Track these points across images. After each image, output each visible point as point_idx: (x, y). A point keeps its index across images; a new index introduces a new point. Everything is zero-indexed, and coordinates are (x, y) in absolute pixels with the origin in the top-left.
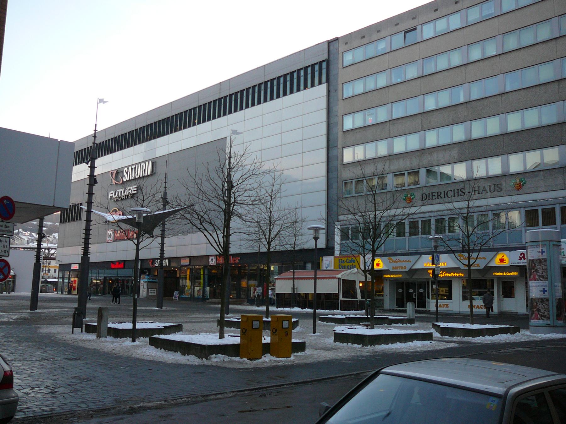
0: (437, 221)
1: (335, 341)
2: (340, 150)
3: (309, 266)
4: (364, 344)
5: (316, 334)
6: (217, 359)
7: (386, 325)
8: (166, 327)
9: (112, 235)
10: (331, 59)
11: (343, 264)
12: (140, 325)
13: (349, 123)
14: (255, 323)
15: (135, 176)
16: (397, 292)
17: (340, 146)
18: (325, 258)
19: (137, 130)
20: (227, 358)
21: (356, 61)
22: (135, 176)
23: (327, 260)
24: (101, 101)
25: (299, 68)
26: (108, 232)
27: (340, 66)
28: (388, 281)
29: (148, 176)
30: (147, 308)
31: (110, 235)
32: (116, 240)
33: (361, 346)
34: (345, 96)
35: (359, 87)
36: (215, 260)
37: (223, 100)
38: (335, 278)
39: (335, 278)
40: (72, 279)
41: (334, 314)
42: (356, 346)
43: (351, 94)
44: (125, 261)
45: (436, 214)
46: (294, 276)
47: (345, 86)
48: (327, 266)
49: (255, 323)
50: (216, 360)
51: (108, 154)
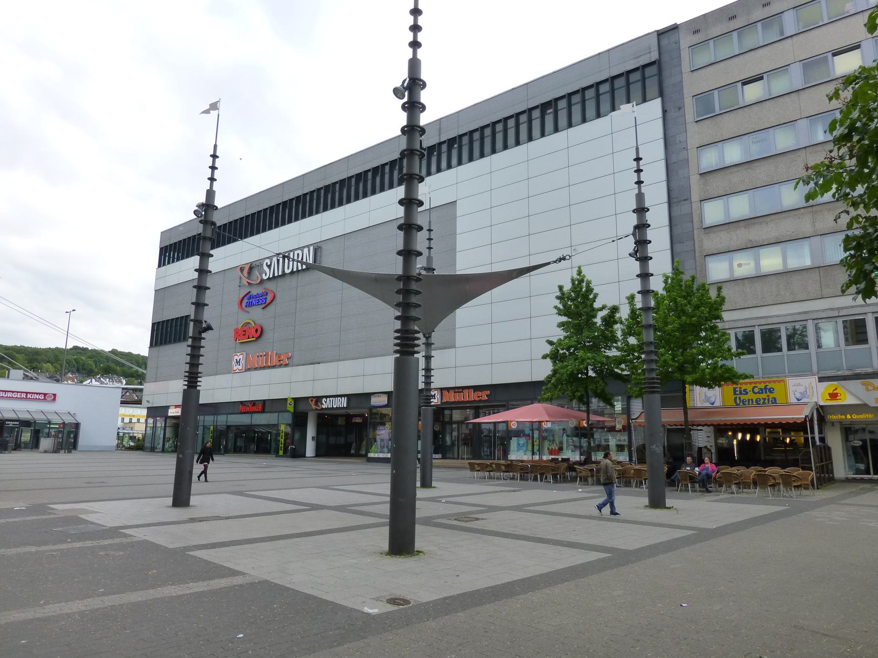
0: (764, 334)
2: (695, 206)
10: (665, 58)
11: (743, 397)
15: (283, 271)
17: (695, 197)
19: (247, 217)
22: (283, 271)
25: (585, 85)
26: (236, 357)
28: (838, 426)
29: (279, 276)
31: (238, 362)
44: (264, 401)
45: (763, 322)
48: (798, 395)
51: (270, 228)
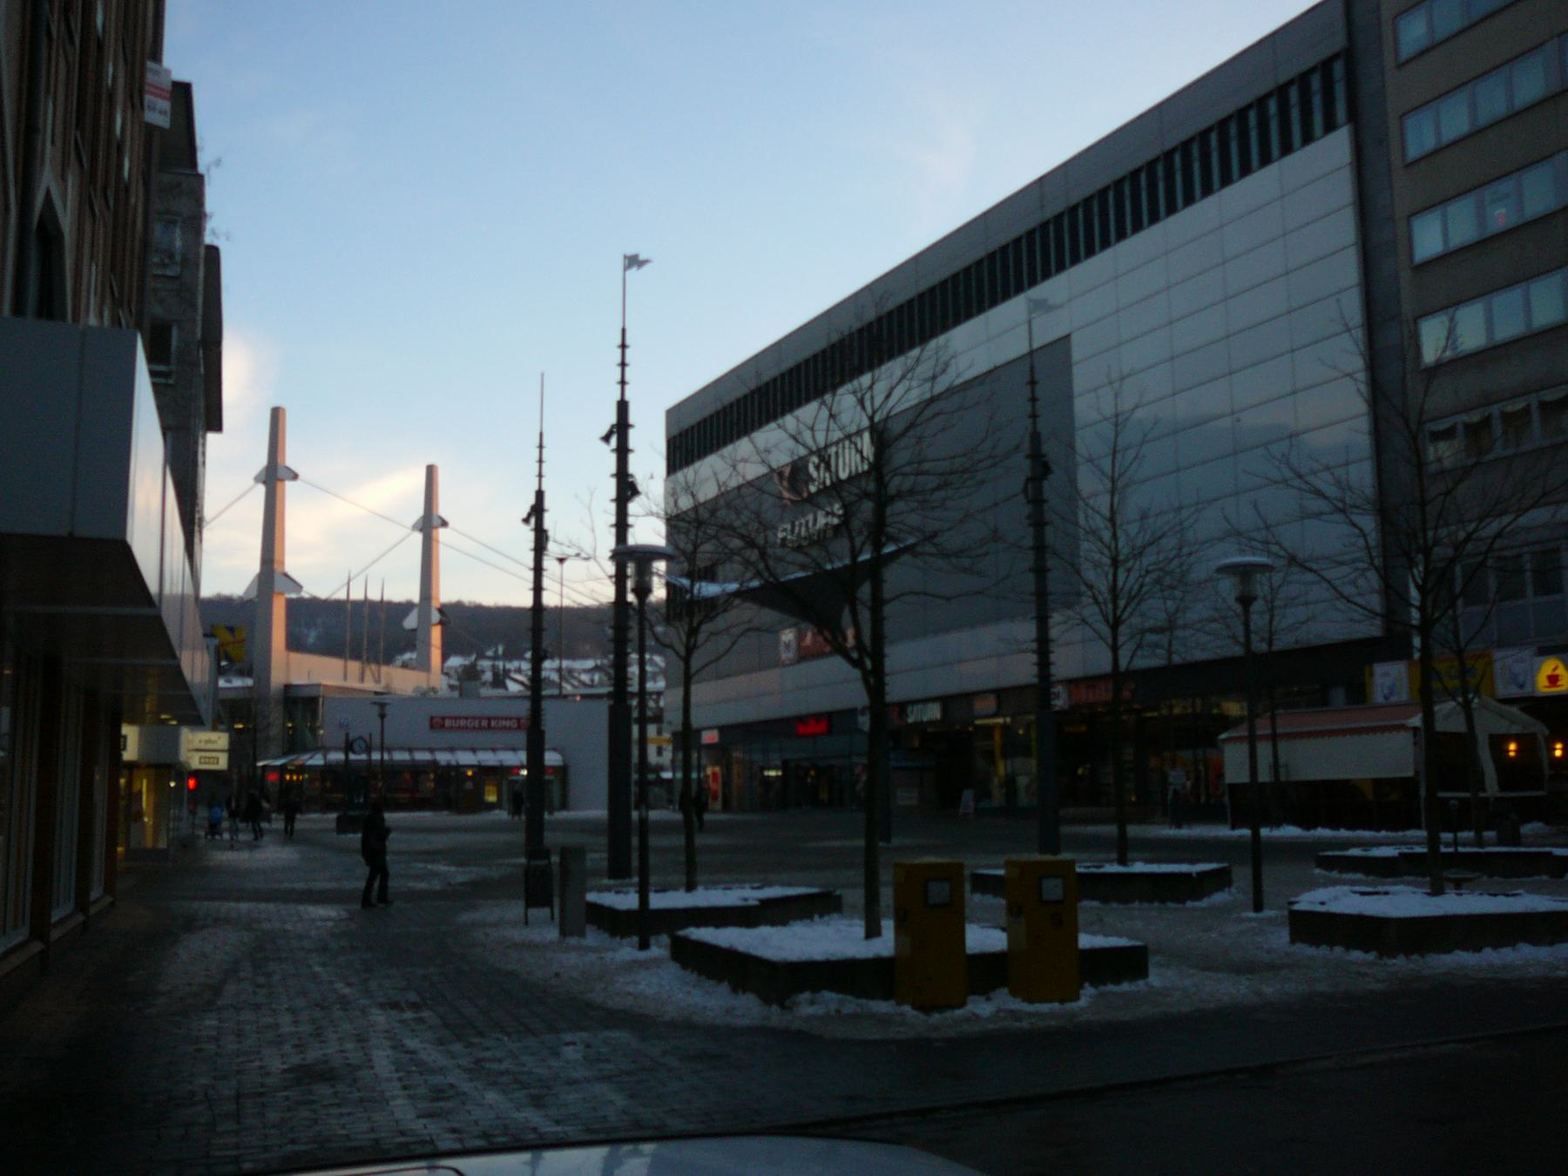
1: (1293, 941)
3: (1339, 696)
4: (1386, 951)
5: (1268, 913)
6: (813, 1007)
7: (1545, 878)
8: (766, 903)
9: (794, 645)
12: (657, 901)
13: (1429, 239)
14: (934, 887)
16: (284, 724)
18: (1380, 669)
20: (851, 1005)
21: (1439, 36)
23: (1386, 674)
24: (633, 261)
27: (1389, 62)
30: (1185, 832)
31: (787, 646)
32: (804, 655)
33: (1371, 956)
34: (1413, 152)
35: (1455, 119)
36: (1064, 696)
37: (1052, 228)
38: (1402, 727)
39: (1402, 727)
40: (709, 771)
41: (1367, 844)
42: (1357, 955)
43: (1429, 143)
46: (1274, 728)
47: (1410, 122)
49: (934, 887)
50: (811, 1010)
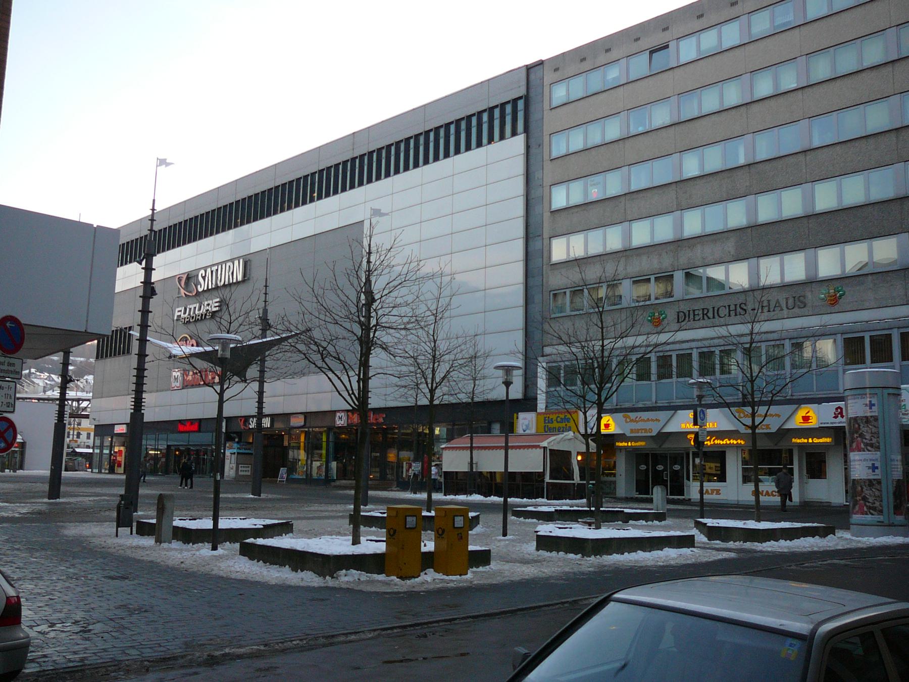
0: (702, 355)
1: (538, 549)
2: (546, 242)
3: (496, 428)
4: (585, 554)
5: (508, 537)
6: (348, 577)
7: (620, 522)
8: (266, 527)
9: (180, 378)
10: (532, 94)
11: (550, 425)
12: (225, 523)
13: (560, 198)
14: (409, 519)
15: (216, 284)
16: (638, 470)
17: (546, 235)
18: (522, 415)
19: (219, 209)
20: (364, 576)
21: (572, 98)
22: (216, 284)
23: (525, 419)
24: (162, 162)
25: (480, 109)
26: (174, 374)
27: (546, 106)
28: (624, 452)
29: (238, 283)
30: (237, 496)
31: (176, 379)
32: (186, 385)
33: (579, 556)
34: (555, 154)
35: (576, 141)
36: (345, 418)
37: (357, 161)
38: (538, 447)
39: (538, 447)
40: (116, 449)
41: (536, 505)
42: (571, 556)
43: (563, 151)
44: (200, 420)
45: (700, 344)
46: (472, 444)
47: (554, 139)
48: (524, 427)
49: (409, 519)
50: (346, 579)
51: (174, 247)
